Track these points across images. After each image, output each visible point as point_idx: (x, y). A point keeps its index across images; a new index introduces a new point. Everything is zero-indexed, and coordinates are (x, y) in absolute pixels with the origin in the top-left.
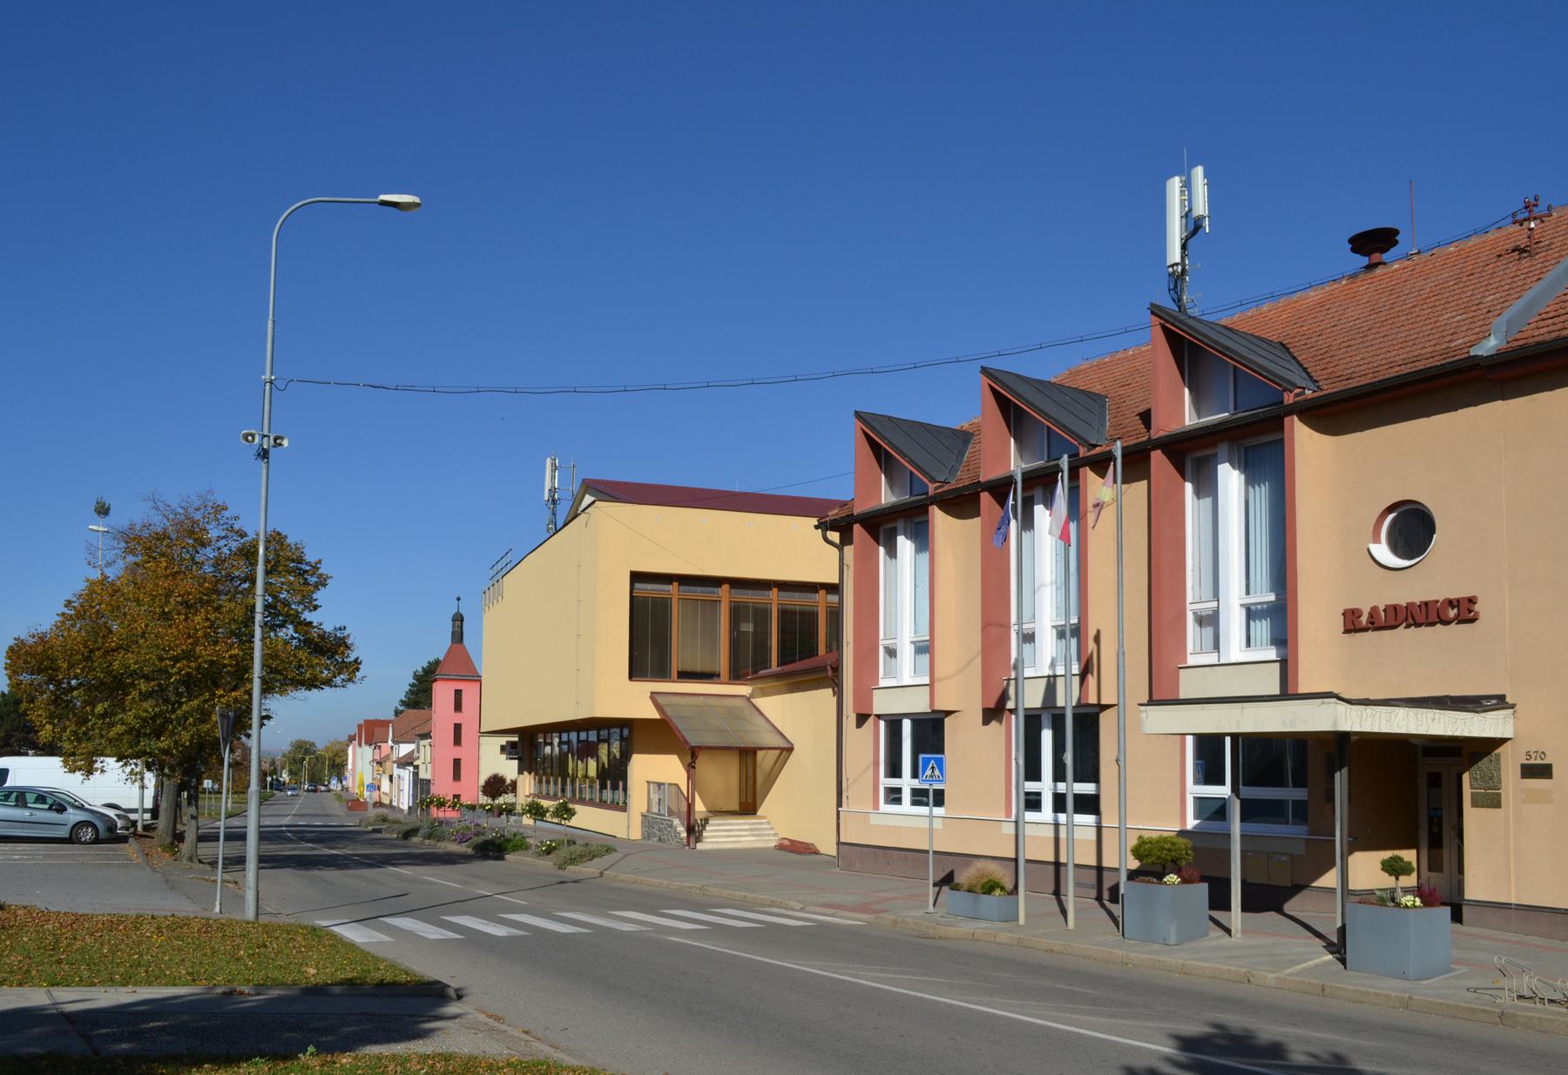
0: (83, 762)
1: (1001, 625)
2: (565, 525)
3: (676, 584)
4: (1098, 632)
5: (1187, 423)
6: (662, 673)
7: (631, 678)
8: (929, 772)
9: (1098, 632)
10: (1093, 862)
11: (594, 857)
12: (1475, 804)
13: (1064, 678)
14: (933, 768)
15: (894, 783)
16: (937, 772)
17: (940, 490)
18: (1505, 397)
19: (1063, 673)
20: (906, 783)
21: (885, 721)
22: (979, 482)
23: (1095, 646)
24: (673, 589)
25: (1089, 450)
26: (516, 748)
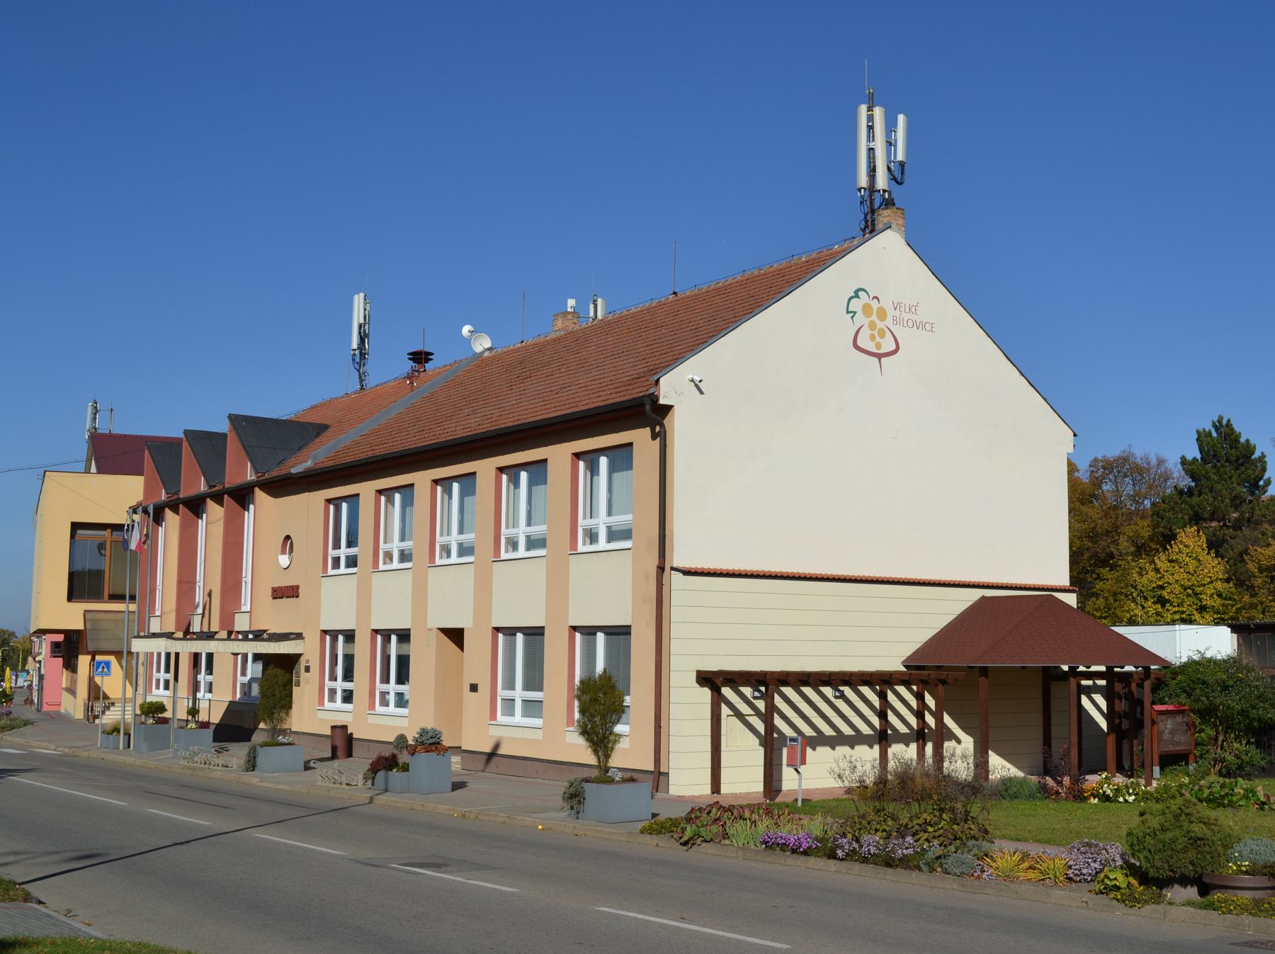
0: (1206, 702)
1: (188, 582)
2: (902, 174)
3: (109, 530)
4: (211, 591)
5: (249, 478)
6: (96, 595)
7: (70, 599)
8: (100, 670)
9: (211, 591)
10: (650, 767)
11: (13, 728)
12: (295, 686)
13: (249, 614)
14: (103, 667)
15: (508, 694)
16: (106, 670)
17: (171, 499)
18: (310, 491)
19: (160, 614)
20: (519, 694)
21: (344, 636)
22: (179, 498)
23: (208, 599)
24: (107, 533)
25: (210, 489)
26: (59, 647)
